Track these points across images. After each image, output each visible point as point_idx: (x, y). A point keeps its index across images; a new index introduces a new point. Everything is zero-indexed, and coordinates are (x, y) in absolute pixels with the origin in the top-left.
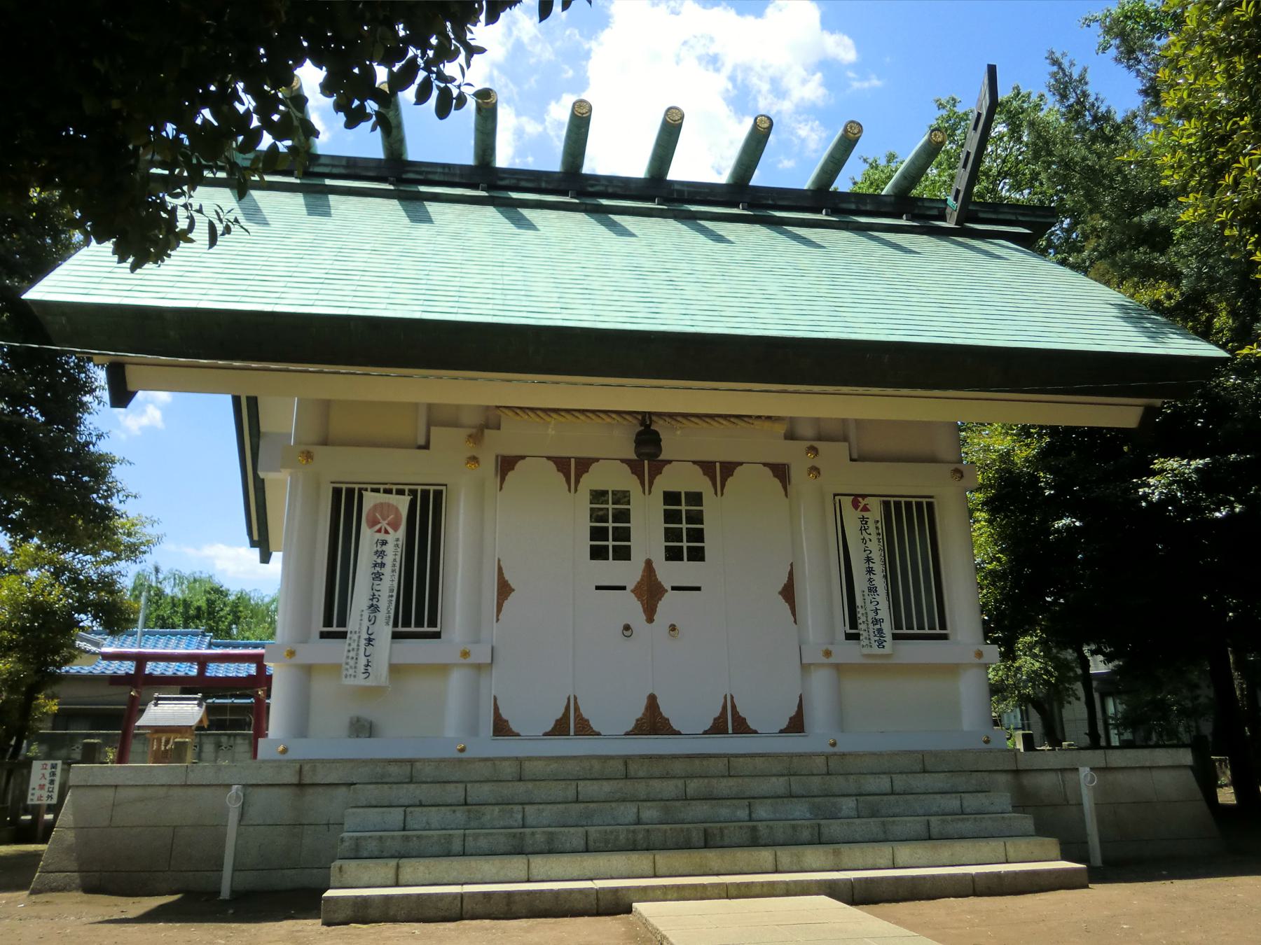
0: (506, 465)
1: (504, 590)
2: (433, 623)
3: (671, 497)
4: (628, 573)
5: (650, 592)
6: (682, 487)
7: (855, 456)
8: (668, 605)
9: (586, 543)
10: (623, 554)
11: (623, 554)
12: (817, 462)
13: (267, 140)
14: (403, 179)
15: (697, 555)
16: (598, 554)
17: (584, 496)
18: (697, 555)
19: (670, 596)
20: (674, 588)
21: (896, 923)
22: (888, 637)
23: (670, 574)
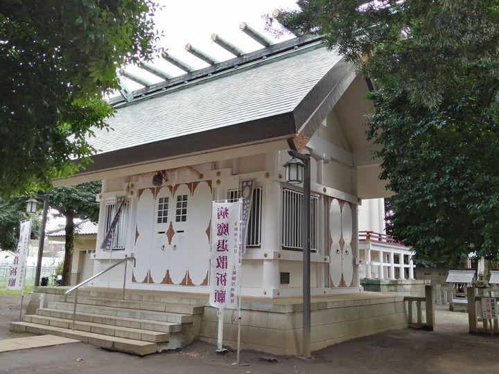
0: (141, 192)
1: (137, 234)
2: (257, 243)
3: (161, 200)
4: (165, 227)
5: (170, 233)
6: (182, 194)
7: (234, 173)
8: (176, 236)
9: (157, 217)
10: (165, 220)
11: (165, 220)
12: (219, 178)
13: (474, 11)
14: (142, 66)
15: (184, 219)
16: (159, 221)
17: (158, 200)
18: (184, 219)
19: (176, 234)
20: (178, 232)
21: (366, 337)
22: (245, 247)
23: (177, 226)
